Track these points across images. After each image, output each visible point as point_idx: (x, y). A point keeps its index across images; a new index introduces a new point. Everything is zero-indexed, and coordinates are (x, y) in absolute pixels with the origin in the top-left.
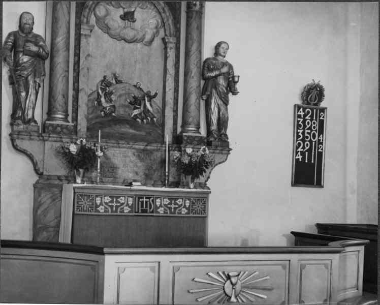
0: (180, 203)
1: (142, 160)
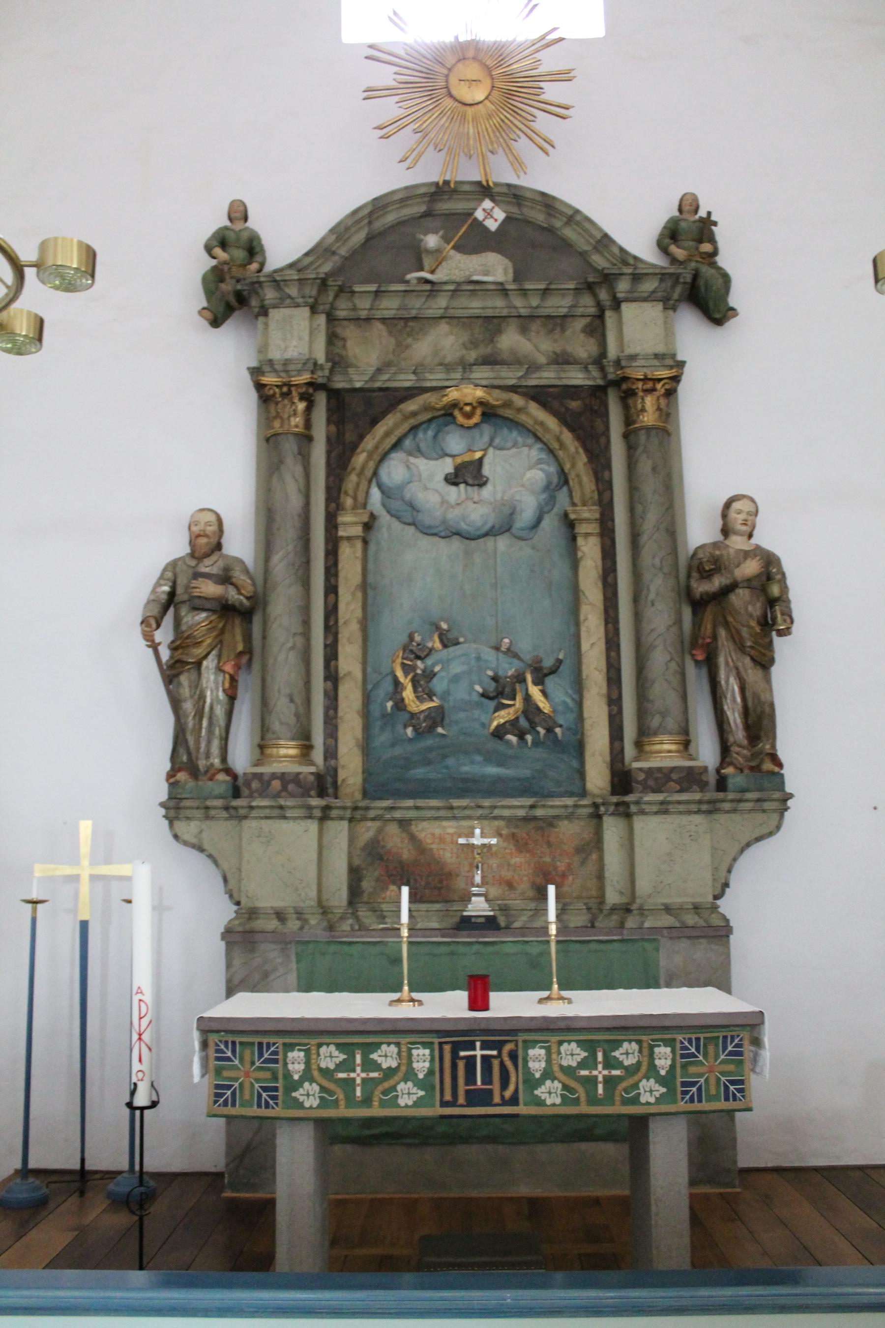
0: (629, 1061)
1: (521, 845)
